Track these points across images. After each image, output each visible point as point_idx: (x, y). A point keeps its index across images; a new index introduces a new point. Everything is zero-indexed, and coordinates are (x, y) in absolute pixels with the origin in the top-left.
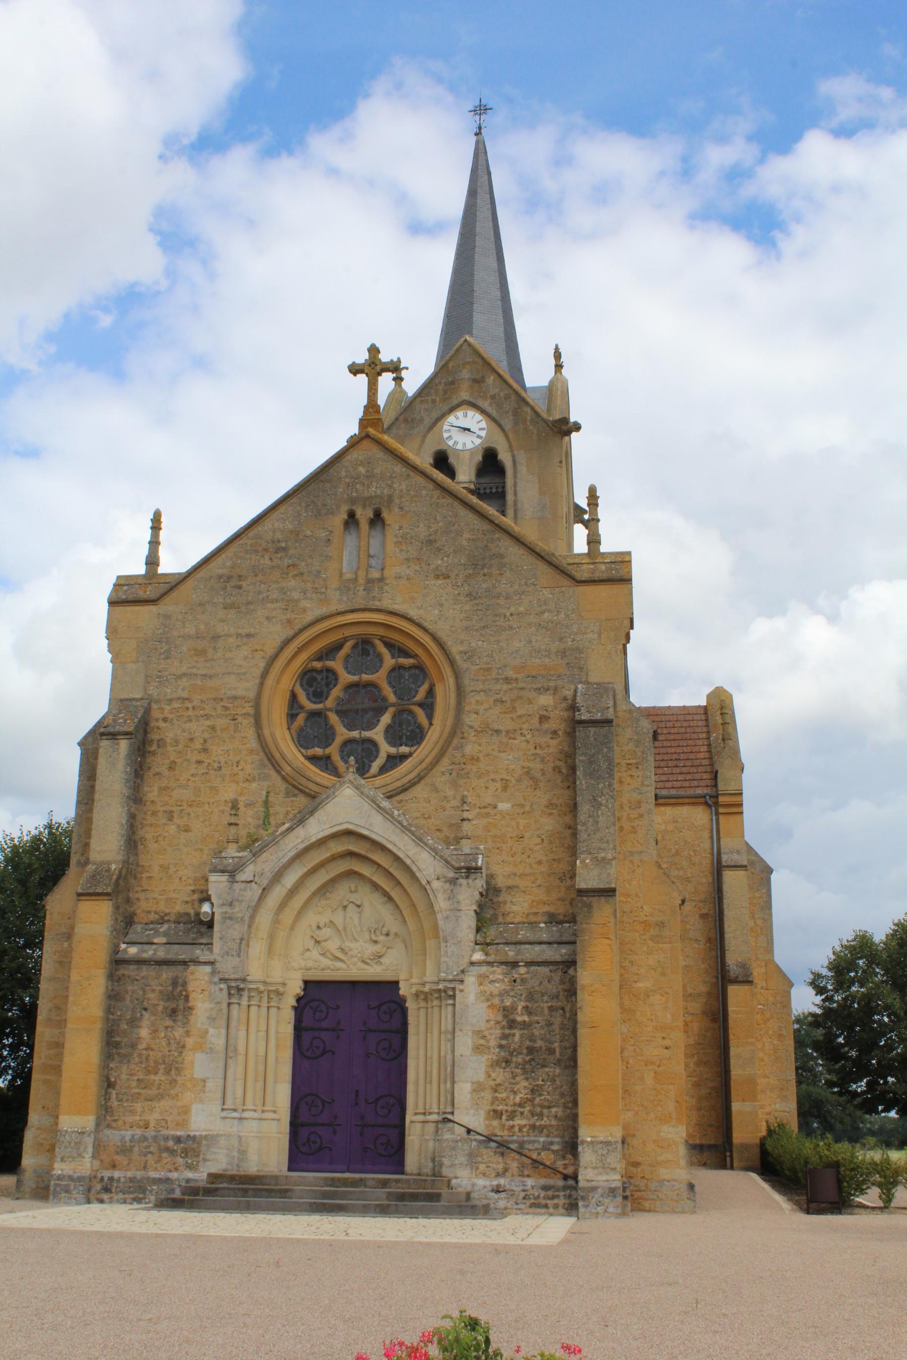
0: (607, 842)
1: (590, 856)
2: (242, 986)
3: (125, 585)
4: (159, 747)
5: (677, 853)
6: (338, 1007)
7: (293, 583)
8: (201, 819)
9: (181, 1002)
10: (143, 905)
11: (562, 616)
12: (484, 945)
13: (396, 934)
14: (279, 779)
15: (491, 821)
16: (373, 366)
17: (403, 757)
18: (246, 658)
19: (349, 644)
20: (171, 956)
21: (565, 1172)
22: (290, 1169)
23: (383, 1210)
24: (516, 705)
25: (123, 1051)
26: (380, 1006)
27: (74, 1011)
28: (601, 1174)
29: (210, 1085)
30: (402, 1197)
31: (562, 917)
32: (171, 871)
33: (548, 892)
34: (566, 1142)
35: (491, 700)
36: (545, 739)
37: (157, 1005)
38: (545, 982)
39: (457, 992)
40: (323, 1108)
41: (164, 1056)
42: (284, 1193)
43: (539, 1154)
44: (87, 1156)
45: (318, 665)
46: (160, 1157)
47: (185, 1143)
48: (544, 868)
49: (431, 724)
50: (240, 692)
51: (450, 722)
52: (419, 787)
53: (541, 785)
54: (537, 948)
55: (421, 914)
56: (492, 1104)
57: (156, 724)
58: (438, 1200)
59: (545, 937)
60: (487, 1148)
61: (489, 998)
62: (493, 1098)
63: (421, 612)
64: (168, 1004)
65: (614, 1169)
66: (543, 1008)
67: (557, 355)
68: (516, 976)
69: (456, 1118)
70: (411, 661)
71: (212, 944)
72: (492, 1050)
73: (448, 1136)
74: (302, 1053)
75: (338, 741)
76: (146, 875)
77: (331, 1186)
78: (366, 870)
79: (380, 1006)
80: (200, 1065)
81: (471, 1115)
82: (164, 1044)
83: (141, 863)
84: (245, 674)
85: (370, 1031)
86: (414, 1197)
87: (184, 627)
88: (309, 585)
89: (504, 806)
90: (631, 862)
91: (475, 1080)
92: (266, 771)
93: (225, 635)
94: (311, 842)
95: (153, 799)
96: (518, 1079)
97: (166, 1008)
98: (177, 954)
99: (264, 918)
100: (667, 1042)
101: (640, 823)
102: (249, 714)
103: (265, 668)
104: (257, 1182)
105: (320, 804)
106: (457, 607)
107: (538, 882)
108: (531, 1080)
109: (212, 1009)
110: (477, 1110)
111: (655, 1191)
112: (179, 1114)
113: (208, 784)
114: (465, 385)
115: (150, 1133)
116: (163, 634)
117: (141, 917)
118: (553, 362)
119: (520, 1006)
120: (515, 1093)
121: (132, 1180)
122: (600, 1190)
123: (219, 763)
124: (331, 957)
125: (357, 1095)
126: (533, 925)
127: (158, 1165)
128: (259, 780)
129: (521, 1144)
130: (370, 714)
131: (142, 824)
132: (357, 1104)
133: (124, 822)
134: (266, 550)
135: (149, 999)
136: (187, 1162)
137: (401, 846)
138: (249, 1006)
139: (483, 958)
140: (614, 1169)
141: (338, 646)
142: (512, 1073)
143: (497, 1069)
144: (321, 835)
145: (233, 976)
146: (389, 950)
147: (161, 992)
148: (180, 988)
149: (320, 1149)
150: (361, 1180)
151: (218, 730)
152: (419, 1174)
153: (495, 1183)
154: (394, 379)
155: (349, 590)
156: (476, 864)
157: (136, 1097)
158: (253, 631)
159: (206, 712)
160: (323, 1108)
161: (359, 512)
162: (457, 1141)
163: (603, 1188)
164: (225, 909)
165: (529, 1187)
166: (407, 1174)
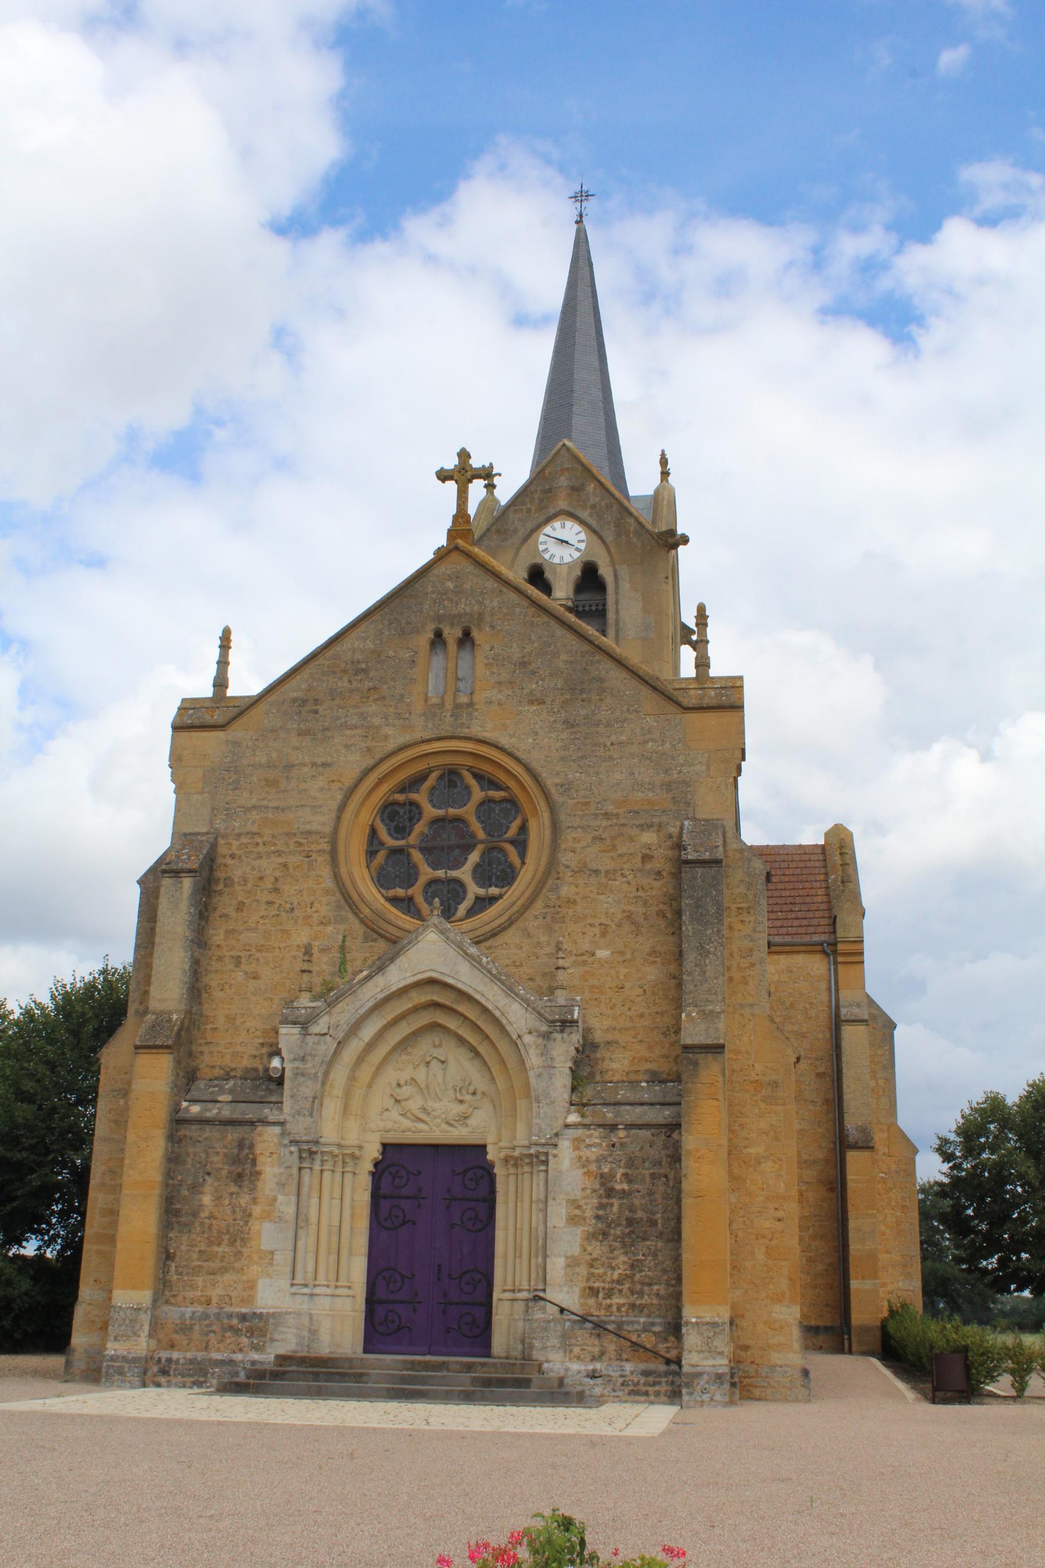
0: (716, 993)
1: (696, 1009)
2: (314, 1149)
4: (225, 886)
5: (792, 1005)
7: (373, 708)
8: (272, 966)
9: (248, 1166)
10: (207, 1059)
12: (580, 1106)
13: (483, 1093)
14: (357, 921)
15: (588, 969)
16: (463, 472)
17: (493, 900)
18: (321, 789)
19: (434, 775)
21: (668, 1356)
22: (365, 1351)
23: (468, 1397)
24: (617, 843)
25: (183, 1219)
26: (465, 1172)
28: (706, 1358)
29: (278, 1257)
30: (488, 1383)
31: (665, 1076)
33: (650, 1048)
34: (669, 1323)
35: (589, 837)
38: (647, 1147)
39: (550, 1157)
41: (228, 1226)
42: (359, 1377)
43: (639, 1336)
44: (142, 1334)
45: (400, 797)
46: (223, 1336)
49: (523, 863)
50: (315, 827)
51: (544, 861)
53: (644, 930)
54: (638, 1109)
56: (588, 1280)
57: (223, 861)
58: (529, 1387)
59: (646, 1097)
60: (582, 1328)
61: (583, 1163)
62: (588, 1274)
63: (514, 740)
64: (233, 1168)
65: (722, 1353)
66: (644, 1175)
67: (664, 461)
68: (614, 1140)
69: (548, 1295)
70: (502, 794)
71: (282, 1103)
72: (588, 1221)
74: (379, 1223)
75: (422, 880)
77: (411, 1369)
78: (452, 1023)
79: (465, 1172)
80: (268, 1236)
82: (228, 1212)
83: (205, 1013)
84: (320, 806)
86: (502, 1383)
87: (254, 755)
88: (391, 710)
89: (603, 954)
90: (742, 1015)
91: (569, 1254)
92: (343, 913)
93: (299, 764)
96: (616, 1253)
99: (339, 1075)
101: (751, 973)
102: (324, 851)
105: (402, 949)
107: (640, 1037)
108: (630, 1255)
109: (281, 1174)
110: (571, 1287)
111: (766, 1377)
112: (244, 1289)
113: (280, 927)
114: (563, 494)
115: (213, 1310)
120: (613, 1269)
121: (192, 1361)
122: (705, 1376)
125: (439, 1270)
126: (634, 1084)
127: (221, 1345)
129: (620, 1325)
134: (345, 671)
135: (212, 1163)
136: (252, 1342)
137: (490, 997)
138: (322, 1171)
139: (579, 1119)
141: (422, 778)
142: (610, 1246)
143: (594, 1243)
145: (304, 1138)
146: (476, 1111)
147: (225, 1155)
148: (246, 1151)
149: (399, 1328)
150: (444, 1363)
152: (507, 1358)
153: (590, 1367)
154: (486, 486)
155: (434, 715)
156: (572, 1017)
157: (196, 1271)
158: (329, 760)
159: (278, 848)
161: (446, 632)
162: (549, 1322)
164: (297, 1064)
165: (627, 1373)
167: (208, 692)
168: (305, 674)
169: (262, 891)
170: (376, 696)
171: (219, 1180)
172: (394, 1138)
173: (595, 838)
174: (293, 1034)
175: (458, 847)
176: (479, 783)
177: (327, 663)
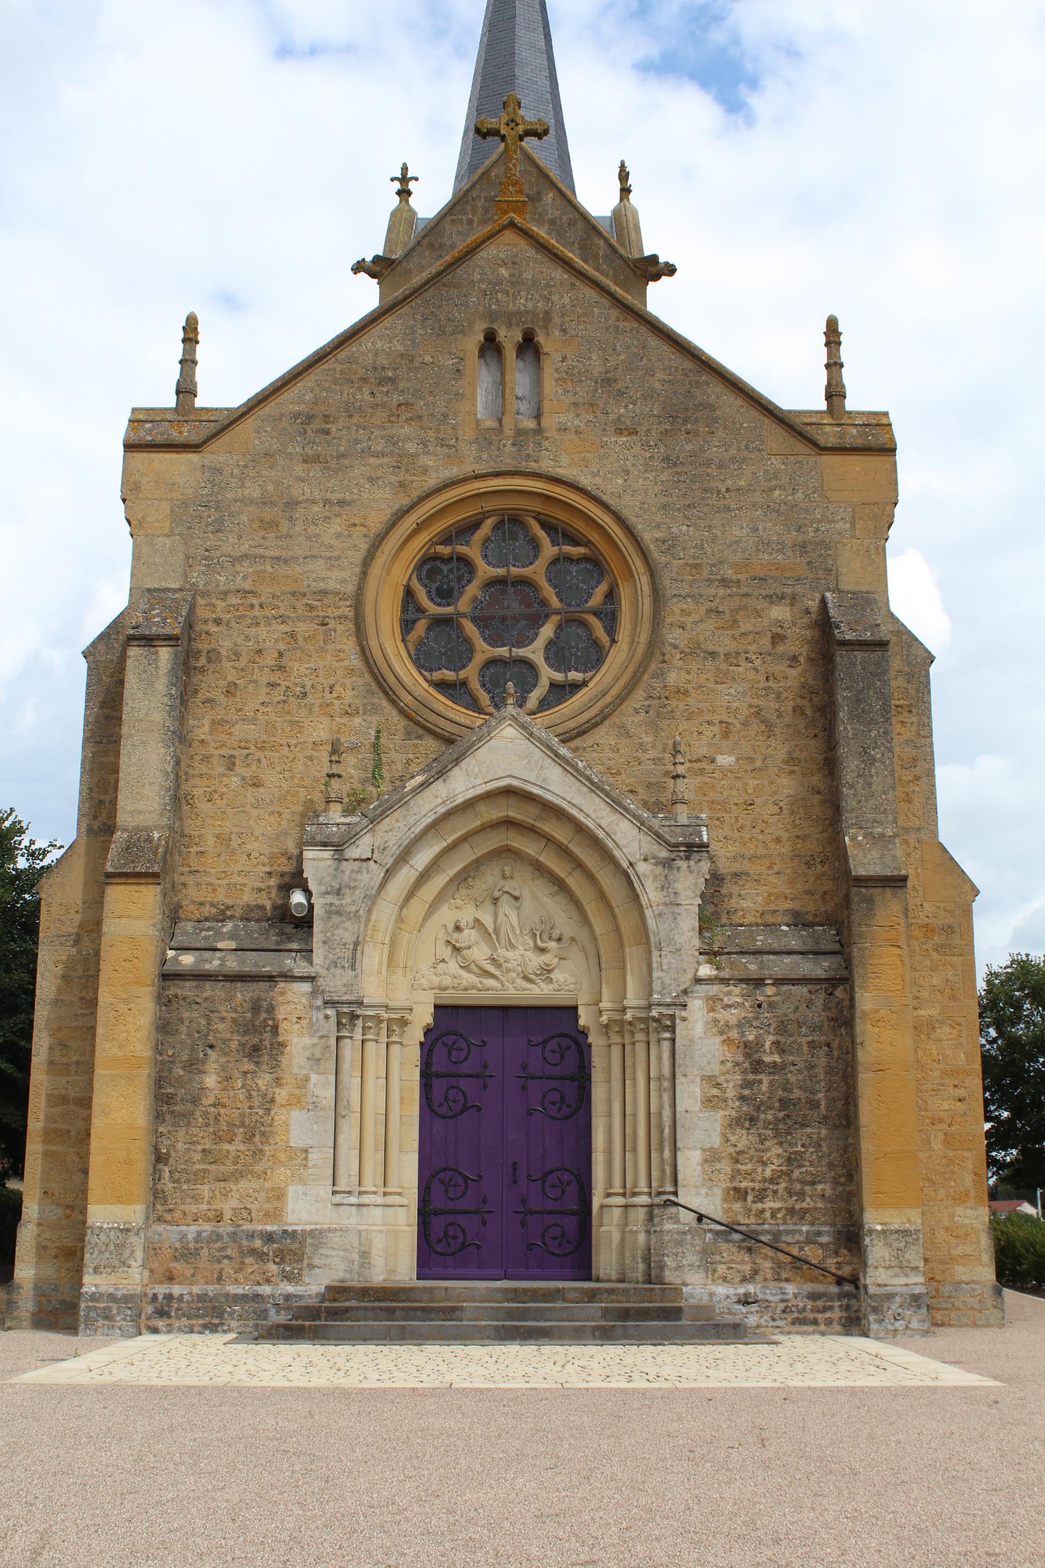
0: (885, 812)
3: (146, 422)
6: (484, 1043)
10: (192, 893)
11: (800, 495)
12: (710, 954)
13: (573, 939)
14: (394, 712)
15: (707, 780)
16: (512, 125)
17: (576, 687)
18: (339, 536)
19: (489, 523)
20: (248, 968)
21: (839, 1273)
22: (418, 1279)
23: (605, 1335)
25: (178, 1108)
27: (105, 1049)
28: (896, 1276)
29: (314, 1156)
30: (625, 1315)
31: (811, 918)
32: (234, 844)
33: (791, 882)
34: (839, 1232)
35: (702, 609)
36: (780, 668)
37: (230, 1040)
38: (803, 1008)
39: (678, 1021)
40: (466, 1188)
41: (242, 1115)
42: (450, 1313)
43: (801, 1249)
45: (444, 550)
46: (243, 1263)
47: (280, 1242)
48: (785, 849)
49: (614, 641)
50: (332, 585)
51: (644, 637)
52: (602, 730)
53: (777, 731)
54: (787, 960)
55: (617, 911)
56: (732, 1179)
57: (205, 628)
59: (794, 944)
60: (728, 1241)
61: (723, 1029)
63: (598, 480)
64: (247, 1038)
65: (915, 1269)
66: (800, 1044)
67: (624, 175)
68: (761, 998)
69: (681, 1200)
70: (582, 550)
71: (311, 951)
72: (730, 1103)
73: (668, 1226)
75: (478, 660)
76: (195, 849)
77: (513, 1300)
78: (530, 847)
80: (298, 1128)
81: (702, 1194)
83: (186, 832)
84: (338, 558)
85: (532, 1078)
87: (242, 486)
88: (431, 433)
89: (725, 760)
90: (906, 842)
92: (376, 701)
94: (456, 803)
95: (203, 737)
96: (768, 1143)
97: (243, 1045)
98: (256, 964)
99: (385, 913)
100: (961, 1092)
101: (917, 789)
103: (369, 551)
104: (403, 1298)
105: (469, 748)
106: (650, 476)
107: (776, 868)
108: (786, 1146)
109: (314, 1046)
111: (950, 1297)
112: (268, 1200)
113: (288, 718)
115: (225, 1228)
116: (211, 495)
117: (189, 909)
118: (617, 185)
119: (769, 1040)
120: (764, 1164)
121: (201, 1298)
122: (897, 1298)
123: (303, 687)
124: (477, 971)
125: (515, 1170)
126: (771, 927)
127: (240, 1276)
128: (364, 713)
129: (777, 1235)
130: (523, 623)
131: (186, 774)
132: (515, 1182)
133: (169, 770)
134: (365, 380)
135: (216, 1031)
136: (283, 1270)
137: (590, 812)
139: (714, 973)
140: (915, 1269)
141: (473, 525)
142: (760, 1135)
144: (471, 794)
145: (344, 998)
146: (562, 961)
147: (234, 1020)
148: (264, 1015)
149: (464, 1246)
150: (558, 1290)
151: (300, 639)
153: (742, 1291)
154: (399, 193)
156: (701, 839)
157: (200, 1177)
158: (348, 497)
159: (281, 612)
160: (466, 1188)
161: (502, 333)
162: (684, 1233)
163: (902, 1295)
164: (329, 899)
165: (790, 1296)
166: (598, 1280)
167: (169, 400)
168: (310, 380)
169: (261, 669)
170: (410, 415)
171: (226, 1054)
172: (452, 997)
173: (709, 611)
174: (322, 860)
175: (525, 617)
176: (549, 535)
177: (339, 368)
